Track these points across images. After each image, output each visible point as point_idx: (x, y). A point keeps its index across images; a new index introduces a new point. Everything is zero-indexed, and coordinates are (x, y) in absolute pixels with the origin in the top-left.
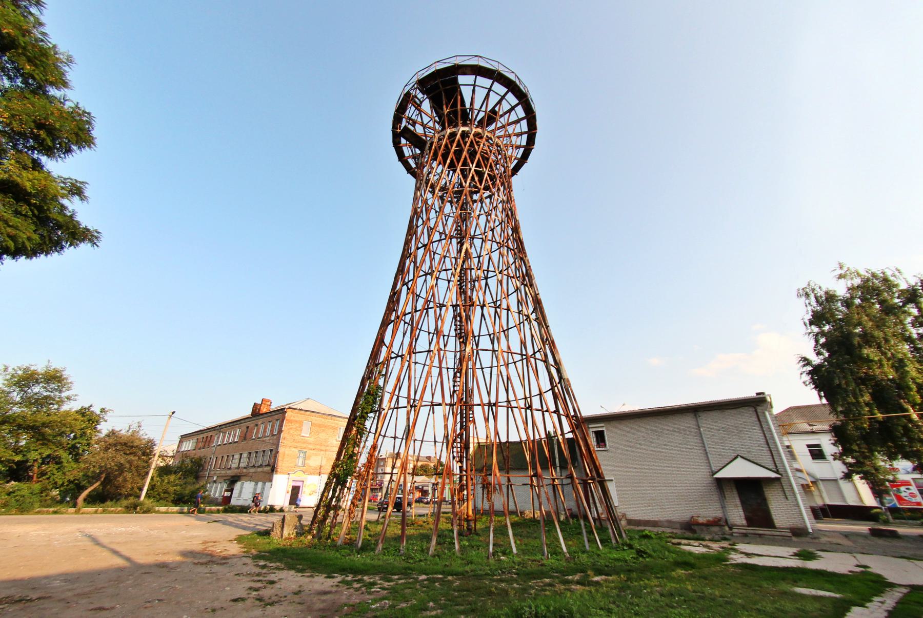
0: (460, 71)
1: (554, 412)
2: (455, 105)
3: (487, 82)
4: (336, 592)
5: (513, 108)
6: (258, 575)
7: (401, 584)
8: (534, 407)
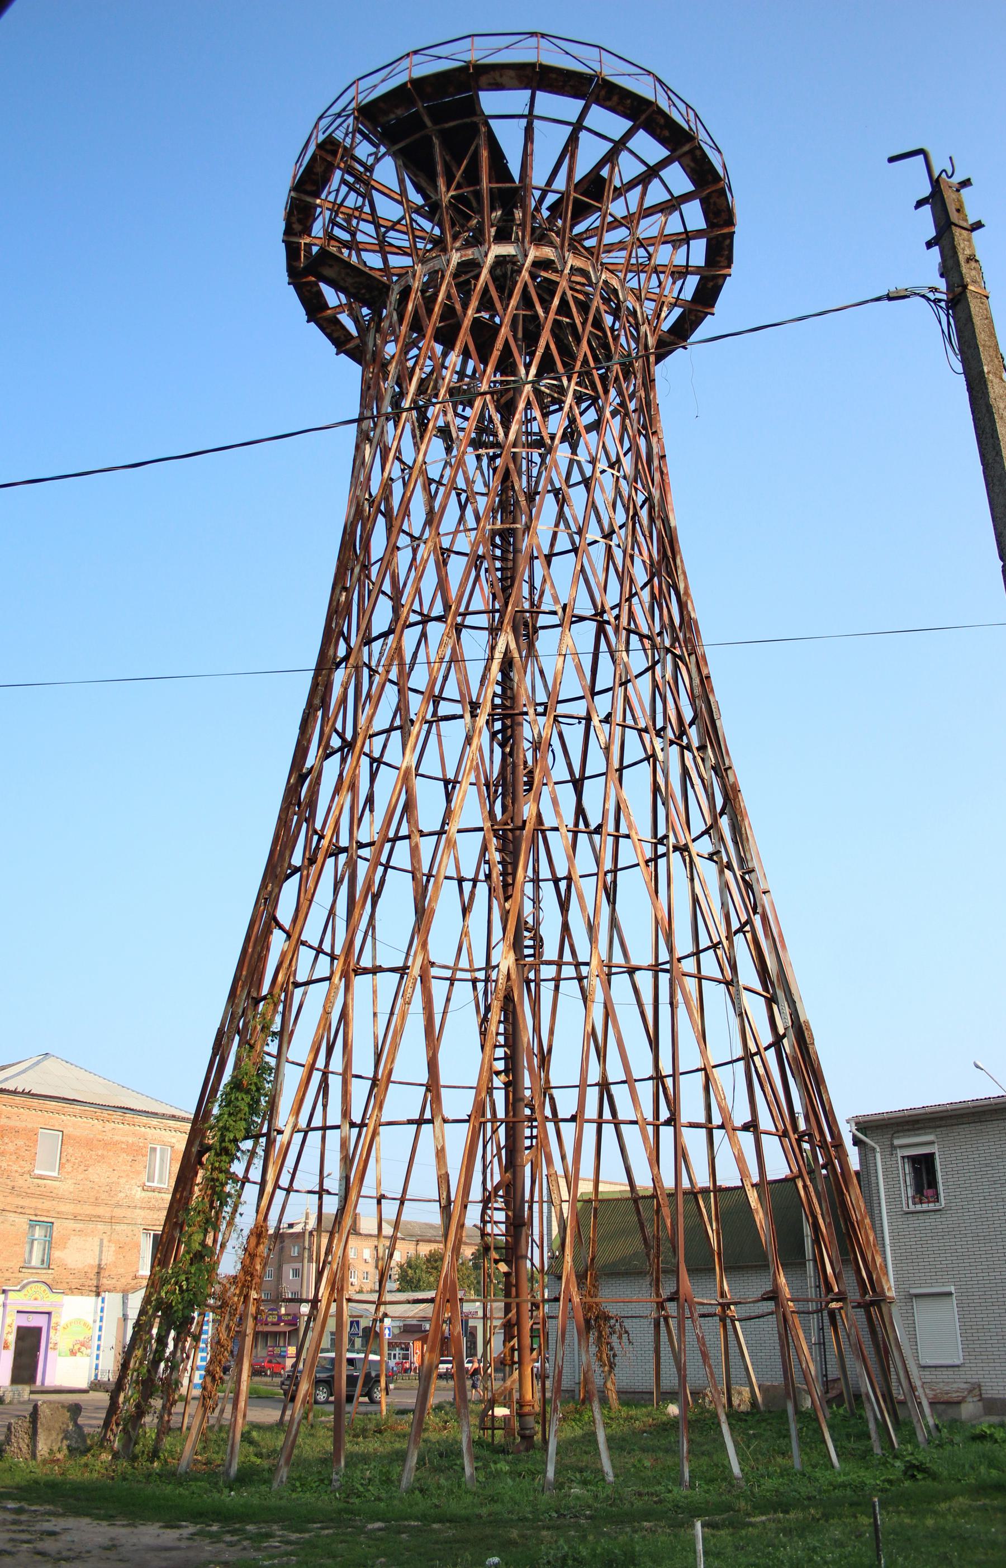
0: (484, 80)
1: (746, 1128)
2: (472, 177)
3: (569, 107)
4: (188, 1548)
5: (652, 172)
6: (14, 1522)
7: (327, 1536)
8: (685, 1118)
